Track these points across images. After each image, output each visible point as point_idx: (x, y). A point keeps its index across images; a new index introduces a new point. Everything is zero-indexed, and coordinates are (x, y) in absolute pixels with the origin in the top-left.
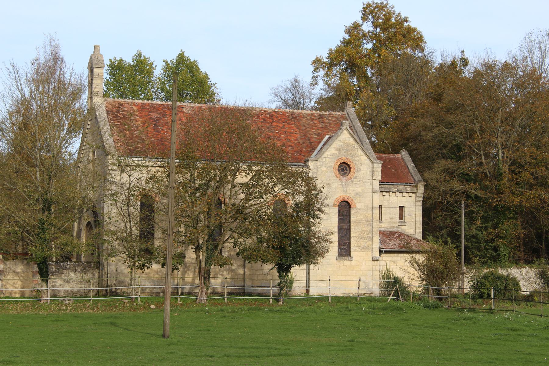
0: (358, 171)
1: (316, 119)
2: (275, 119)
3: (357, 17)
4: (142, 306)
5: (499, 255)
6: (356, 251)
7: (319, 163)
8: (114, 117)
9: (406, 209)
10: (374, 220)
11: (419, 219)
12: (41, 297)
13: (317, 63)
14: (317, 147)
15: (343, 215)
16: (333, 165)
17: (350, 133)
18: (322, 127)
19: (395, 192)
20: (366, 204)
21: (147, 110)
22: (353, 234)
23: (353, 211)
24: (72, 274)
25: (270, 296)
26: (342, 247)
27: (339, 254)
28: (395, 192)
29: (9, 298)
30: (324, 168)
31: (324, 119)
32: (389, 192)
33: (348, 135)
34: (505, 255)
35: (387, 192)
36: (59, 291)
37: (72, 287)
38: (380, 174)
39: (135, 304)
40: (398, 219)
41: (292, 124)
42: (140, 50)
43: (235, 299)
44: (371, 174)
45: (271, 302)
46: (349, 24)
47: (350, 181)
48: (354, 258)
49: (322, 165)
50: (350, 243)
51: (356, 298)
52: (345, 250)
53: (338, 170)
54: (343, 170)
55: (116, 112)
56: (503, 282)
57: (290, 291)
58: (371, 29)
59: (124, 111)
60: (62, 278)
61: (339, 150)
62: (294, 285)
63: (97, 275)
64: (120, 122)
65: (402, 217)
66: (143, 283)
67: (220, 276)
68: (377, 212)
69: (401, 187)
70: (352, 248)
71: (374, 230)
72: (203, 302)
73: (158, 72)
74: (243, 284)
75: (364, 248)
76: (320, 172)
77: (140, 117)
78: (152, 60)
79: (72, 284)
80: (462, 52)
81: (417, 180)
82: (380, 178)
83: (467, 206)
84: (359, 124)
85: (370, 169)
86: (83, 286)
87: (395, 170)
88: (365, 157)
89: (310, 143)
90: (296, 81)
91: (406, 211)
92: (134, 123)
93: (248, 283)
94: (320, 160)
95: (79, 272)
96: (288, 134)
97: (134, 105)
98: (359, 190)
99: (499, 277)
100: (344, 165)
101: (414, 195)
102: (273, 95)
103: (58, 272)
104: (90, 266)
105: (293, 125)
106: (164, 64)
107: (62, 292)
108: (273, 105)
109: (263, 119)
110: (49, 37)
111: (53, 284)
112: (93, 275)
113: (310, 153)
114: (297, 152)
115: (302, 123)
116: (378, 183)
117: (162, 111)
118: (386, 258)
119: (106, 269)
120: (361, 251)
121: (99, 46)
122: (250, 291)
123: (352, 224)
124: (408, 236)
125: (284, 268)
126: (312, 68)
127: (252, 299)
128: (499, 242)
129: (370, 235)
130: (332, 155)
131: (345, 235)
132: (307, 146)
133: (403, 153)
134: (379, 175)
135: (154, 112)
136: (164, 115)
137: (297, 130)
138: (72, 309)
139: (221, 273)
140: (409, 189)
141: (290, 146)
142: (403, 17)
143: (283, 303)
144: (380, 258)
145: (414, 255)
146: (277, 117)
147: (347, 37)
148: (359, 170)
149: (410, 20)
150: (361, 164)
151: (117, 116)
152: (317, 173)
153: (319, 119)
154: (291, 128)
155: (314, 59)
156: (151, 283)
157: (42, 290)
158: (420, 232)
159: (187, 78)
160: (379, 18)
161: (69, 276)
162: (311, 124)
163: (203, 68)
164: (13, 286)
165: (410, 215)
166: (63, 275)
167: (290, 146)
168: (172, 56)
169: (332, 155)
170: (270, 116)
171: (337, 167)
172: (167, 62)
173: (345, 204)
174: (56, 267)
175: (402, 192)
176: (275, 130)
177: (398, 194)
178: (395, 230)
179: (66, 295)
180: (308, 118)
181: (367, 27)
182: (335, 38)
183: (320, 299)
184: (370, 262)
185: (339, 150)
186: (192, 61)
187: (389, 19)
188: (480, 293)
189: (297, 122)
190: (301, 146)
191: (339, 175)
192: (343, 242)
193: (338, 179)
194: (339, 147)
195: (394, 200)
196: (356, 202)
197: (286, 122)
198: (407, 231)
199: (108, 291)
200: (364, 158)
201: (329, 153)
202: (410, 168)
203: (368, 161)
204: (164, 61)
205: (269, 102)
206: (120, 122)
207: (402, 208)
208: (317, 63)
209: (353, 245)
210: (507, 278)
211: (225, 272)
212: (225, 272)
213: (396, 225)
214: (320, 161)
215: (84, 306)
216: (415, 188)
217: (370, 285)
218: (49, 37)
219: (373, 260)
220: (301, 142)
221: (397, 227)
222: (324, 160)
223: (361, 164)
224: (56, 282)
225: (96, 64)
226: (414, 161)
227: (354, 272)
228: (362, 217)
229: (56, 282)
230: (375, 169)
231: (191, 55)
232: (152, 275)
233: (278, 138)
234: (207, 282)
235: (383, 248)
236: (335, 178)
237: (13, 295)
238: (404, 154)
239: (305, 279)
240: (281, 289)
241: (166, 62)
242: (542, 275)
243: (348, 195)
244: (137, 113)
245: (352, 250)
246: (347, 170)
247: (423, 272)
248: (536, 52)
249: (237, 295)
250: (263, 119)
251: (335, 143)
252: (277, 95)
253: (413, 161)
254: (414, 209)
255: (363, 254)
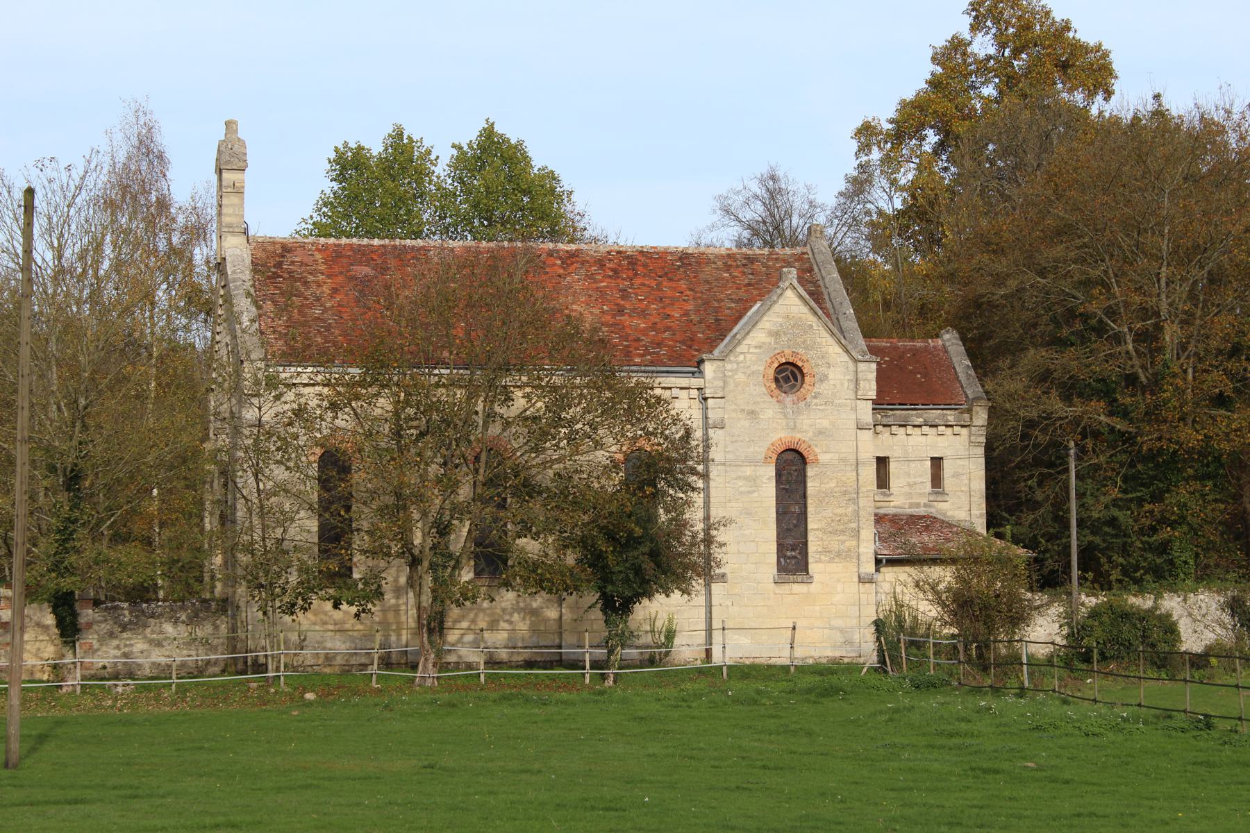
0: (822, 381)
1: (738, 266)
2: (640, 270)
3: (961, 25)
4: (286, 694)
5: (1171, 562)
6: (819, 561)
7: (728, 366)
8: (269, 278)
9: (946, 464)
10: (863, 489)
11: (979, 485)
12: (63, 680)
13: (866, 133)
14: (731, 330)
15: (788, 482)
16: (762, 368)
17: (801, 297)
18: (749, 285)
19: (920, 426)
20: (842, 456)
21: (345, 260)
22: (814, 523)
23: (810, 471)
24: (169, 628)
25: (584, 668)
26: (789, 554)
27: (781, 569)
28: (920, 426)
29: (29, 682)
30: (740, 377)
31: (758, 267)
32: (905, 426)
33: (797, 301)
34: (1186, 562)
35: (900, 426)
36: (139, 665)
37: (169, 656)
38: (874, 386)
39: (272, 690)
40: (928, 487)
41: (679, 280)
42: (399, 123)
43: (505, 676)
44: (852, 386)
45: (587, 681)
46: (941, 42)
47: (802, 404)
48: (816, 577)
49: (737, 370)
50: (806, 544)
51: (785, 669)
52: (793, 557)
53: (777, 380)
54: (787, 380)
55: (274, 266)
56: (1135, 625)
57: (667, 654)
58: (992, 51)
59: (293, 263)
60: (145, 637)
61: (775, 334)
62: (677, 641)
63: (224, 628)
64: (280, 288)
65: (937, 480)
66: (329, 645)
67: (506, 626)
68: (870, 473)
69: (933, 415)
70: (810, 554)
71: (862, 513)
72: (429, 683)
73: (441, 169)
74: (557, 641)
75: (839, 554)
76: (731, 386)
77: (329, 277)
78: (427, 144)
79: (168, 648)
80: (1157, 97)
81: (970, 396)
82: (873, 394)
83: (1082, 450)
84: (836, 275)
85: (851, 376)
86: (194, 653)
87: (924, 376)
88: (838, 350)
89: (717, 320)
90: (773, 178)
91: (948, 468)
92: (313, 289)
93: (569, 638)
94: (732, 358)
95: (183, 622)
96: (668, 301)
97: (318, 250)
98: (825, 423)
99: (1126, 615)
100: (790, 368)
101: (964, 431)
102: (719, 212)
103: (136, 624)
104: (208, 609)
105: (682, 282)
106: (455, 152)
107: (147, 666)
108: (724, 237)
109: (612, 270)
110: (133, 105)
111: (126, 650)
112: (216, 628)
113: (712, 344)
114: (683, 342)
115: (702, 276)
116: (870, 405)
117: (379, 262)
118: (890, 575)
119: (244, 615)
120: (831, 560)
121: (235, 123)
122: (573, 657)
123: (809, 501)
124: (950, 526)
125: (617, 606)
126: (854, 145)
127: (547, 676)
128: (1165, 533)
129: (854, 525)
130: (760, 347)
131: (795, 526)
132: (709, 327)
133: (947, 336)
134: (870, 388)
135: (360, 263)
136: (383, 269)
137: (688, 293)
138: (125, 704)
139: (507, 617)
140: (951, 417)
141: (668, 329)
142: (1058, 19)
143: (615, 682)
144: (879, 577)
145: (926, 568)
146: (645, 266)
147: (939, 70)
148: (824, 378)
149: (1074, 25)
150: (829, 365)
151: (276, 276)
152: (724, 388)
153: (744, 265)
154: (674, 289)
155: (859, 124)
156: (348, 644)
157: (64, 664)
158: (981, 515)
159: (504, 184)
160: (1008, 24)
161: (161, 632)
162: (723, 279)
163: (540, 158)
164: (36, 656)
165: (956, 475)
166: (148, 630)
167: (668, 329)
168: (468, 135)
169: (760, 347)
170: (629, 263)
171: (771, 372)
172: (461, 148)
173: (791, 456)
174: (131, 613)
175: (936, 426)
176: (637, 295)
177: (926, 429)
178: (921, 511)
179: (155, 672)
180: (720, 264)
181: (983, 46)
182: (913, 77)
183: (743, 672)
184: (854, 586)
185: (775, 334)
186: (513, 142)
187: (1028, 27)
188: (1079, 654)
189: (692, 275)
190: (695, 329)
191: (777, 392)
192: (790, 541)
193: (774, 400)
194: (774, 329)
195: (913, 445)
196: (817, 450)
197: (666, 274)
198: (950, 513)
199: (249, 663)
200: (834, 350)
201: (753, 343)
202: (958, 370)
203: (845, 357)
204: (454, 146)
205: (713, 227)
206: (280, 288)
207: (937, 462)
208: (866, 133)
209: (812, 548)
210: (1144, 617)
211: (516, 615)
212: (516, 615)
213: (924, 500)
214: (731, 362)
215: (157, 698)
216: (967, 415)
217: (856, 638)
218: (133, 105)
219: (862, 580)
220: (695, 318)
221: (925, 505)
222: (741, 358)
223: (829, 365)
224: (132, 645)
225: (228, 162)
226: (971, 354)
227: (818, 608)
228: (832, 485)
229: (132, 645)
230: (860, 375)
231: (510, 130)
232: (348, 626)
233: (643, 311)
234: (436, 638)
235: (886, 552)
236: (768, 398)
237: (38, 676)
238: (950, 340)
239: (702, 625)
240: (611, 652)
241: (458, 147)
242: (1234, 606)
243: (798, 436)
244: (323, 267)
245: (810, 560)
246: (796, 380)
247: (943, 605)
248: (1227, 99)
249: (511, 668)
250: (612, 270)
251: (765, 318)
252: (727, 211)
253: (968, 355)
254: (965, 462)
255: (836, 567)
